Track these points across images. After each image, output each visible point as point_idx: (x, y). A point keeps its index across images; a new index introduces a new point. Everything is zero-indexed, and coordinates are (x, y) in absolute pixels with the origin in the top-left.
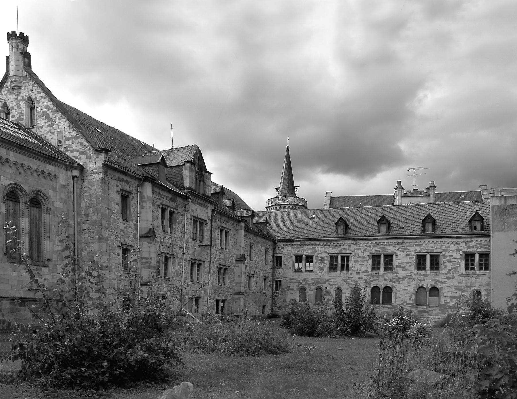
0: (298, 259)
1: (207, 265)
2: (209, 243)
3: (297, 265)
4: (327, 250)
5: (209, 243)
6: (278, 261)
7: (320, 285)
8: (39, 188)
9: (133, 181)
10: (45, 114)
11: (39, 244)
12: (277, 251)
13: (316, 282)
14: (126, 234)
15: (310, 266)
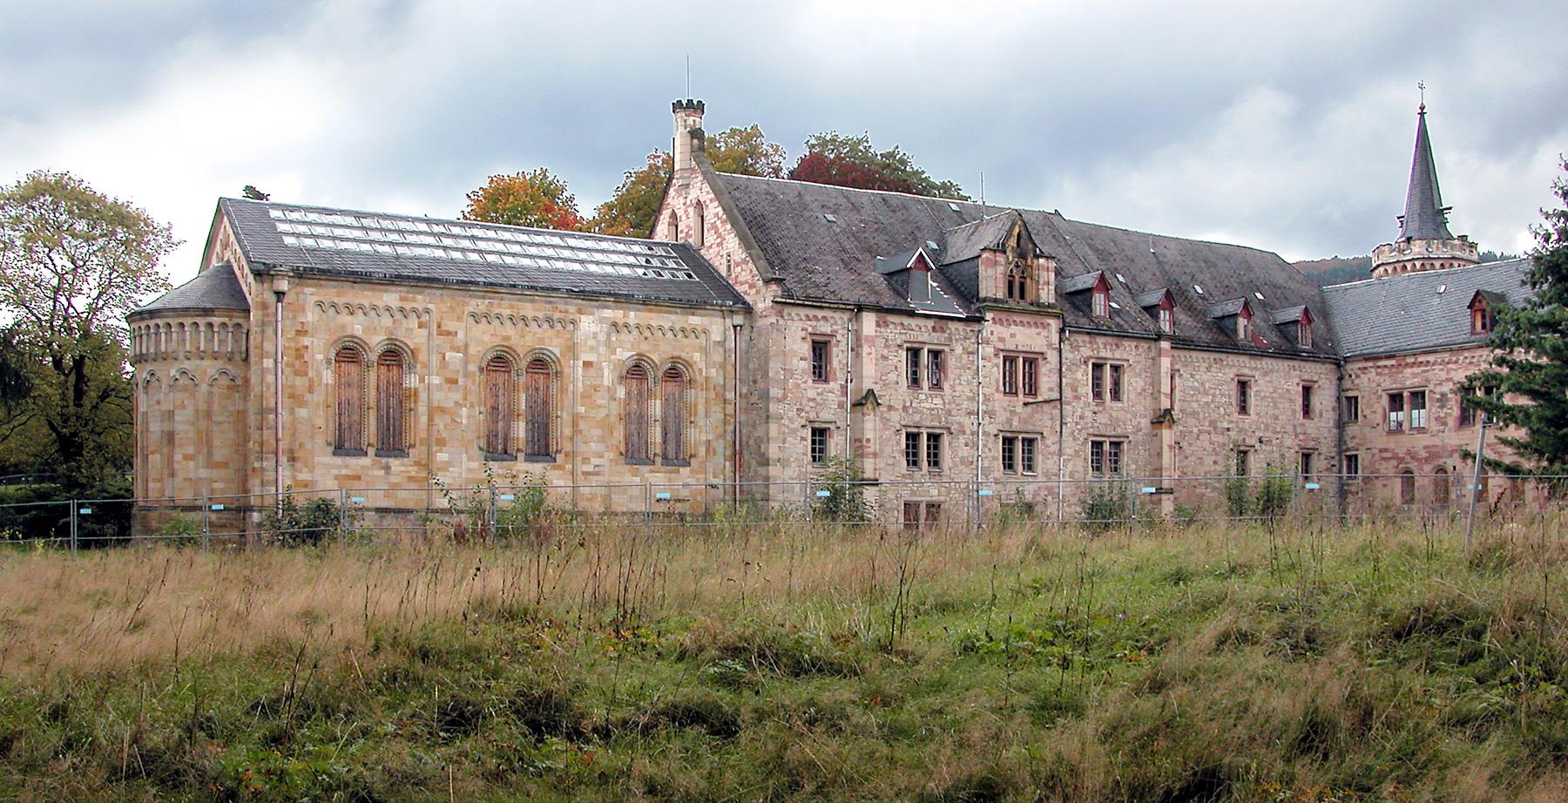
0: (1396, 401)
1: (1051, 439)
2: (1056, 396)
3: (1393, 415)
4: (1453, 374)
5: (1056, 396)
6: (1348, 407)
7: (1440, 462)
8: (676, 354)
9: (838, 315)
10: (714, 226)
11: (679, 435)
12: (1347, 384)
13: (1433, 454)
14: (823, 405)
15: (1420, 417)
